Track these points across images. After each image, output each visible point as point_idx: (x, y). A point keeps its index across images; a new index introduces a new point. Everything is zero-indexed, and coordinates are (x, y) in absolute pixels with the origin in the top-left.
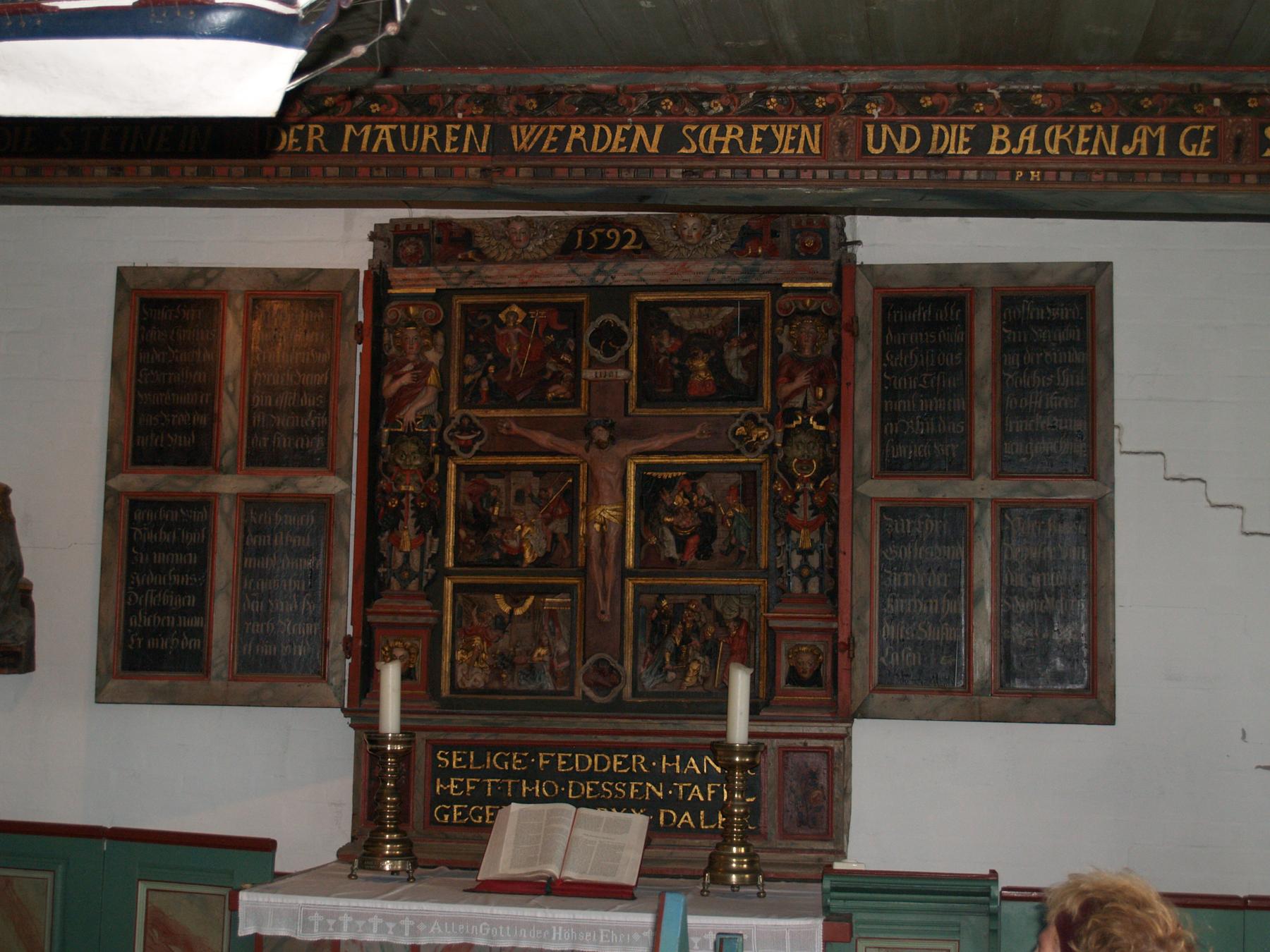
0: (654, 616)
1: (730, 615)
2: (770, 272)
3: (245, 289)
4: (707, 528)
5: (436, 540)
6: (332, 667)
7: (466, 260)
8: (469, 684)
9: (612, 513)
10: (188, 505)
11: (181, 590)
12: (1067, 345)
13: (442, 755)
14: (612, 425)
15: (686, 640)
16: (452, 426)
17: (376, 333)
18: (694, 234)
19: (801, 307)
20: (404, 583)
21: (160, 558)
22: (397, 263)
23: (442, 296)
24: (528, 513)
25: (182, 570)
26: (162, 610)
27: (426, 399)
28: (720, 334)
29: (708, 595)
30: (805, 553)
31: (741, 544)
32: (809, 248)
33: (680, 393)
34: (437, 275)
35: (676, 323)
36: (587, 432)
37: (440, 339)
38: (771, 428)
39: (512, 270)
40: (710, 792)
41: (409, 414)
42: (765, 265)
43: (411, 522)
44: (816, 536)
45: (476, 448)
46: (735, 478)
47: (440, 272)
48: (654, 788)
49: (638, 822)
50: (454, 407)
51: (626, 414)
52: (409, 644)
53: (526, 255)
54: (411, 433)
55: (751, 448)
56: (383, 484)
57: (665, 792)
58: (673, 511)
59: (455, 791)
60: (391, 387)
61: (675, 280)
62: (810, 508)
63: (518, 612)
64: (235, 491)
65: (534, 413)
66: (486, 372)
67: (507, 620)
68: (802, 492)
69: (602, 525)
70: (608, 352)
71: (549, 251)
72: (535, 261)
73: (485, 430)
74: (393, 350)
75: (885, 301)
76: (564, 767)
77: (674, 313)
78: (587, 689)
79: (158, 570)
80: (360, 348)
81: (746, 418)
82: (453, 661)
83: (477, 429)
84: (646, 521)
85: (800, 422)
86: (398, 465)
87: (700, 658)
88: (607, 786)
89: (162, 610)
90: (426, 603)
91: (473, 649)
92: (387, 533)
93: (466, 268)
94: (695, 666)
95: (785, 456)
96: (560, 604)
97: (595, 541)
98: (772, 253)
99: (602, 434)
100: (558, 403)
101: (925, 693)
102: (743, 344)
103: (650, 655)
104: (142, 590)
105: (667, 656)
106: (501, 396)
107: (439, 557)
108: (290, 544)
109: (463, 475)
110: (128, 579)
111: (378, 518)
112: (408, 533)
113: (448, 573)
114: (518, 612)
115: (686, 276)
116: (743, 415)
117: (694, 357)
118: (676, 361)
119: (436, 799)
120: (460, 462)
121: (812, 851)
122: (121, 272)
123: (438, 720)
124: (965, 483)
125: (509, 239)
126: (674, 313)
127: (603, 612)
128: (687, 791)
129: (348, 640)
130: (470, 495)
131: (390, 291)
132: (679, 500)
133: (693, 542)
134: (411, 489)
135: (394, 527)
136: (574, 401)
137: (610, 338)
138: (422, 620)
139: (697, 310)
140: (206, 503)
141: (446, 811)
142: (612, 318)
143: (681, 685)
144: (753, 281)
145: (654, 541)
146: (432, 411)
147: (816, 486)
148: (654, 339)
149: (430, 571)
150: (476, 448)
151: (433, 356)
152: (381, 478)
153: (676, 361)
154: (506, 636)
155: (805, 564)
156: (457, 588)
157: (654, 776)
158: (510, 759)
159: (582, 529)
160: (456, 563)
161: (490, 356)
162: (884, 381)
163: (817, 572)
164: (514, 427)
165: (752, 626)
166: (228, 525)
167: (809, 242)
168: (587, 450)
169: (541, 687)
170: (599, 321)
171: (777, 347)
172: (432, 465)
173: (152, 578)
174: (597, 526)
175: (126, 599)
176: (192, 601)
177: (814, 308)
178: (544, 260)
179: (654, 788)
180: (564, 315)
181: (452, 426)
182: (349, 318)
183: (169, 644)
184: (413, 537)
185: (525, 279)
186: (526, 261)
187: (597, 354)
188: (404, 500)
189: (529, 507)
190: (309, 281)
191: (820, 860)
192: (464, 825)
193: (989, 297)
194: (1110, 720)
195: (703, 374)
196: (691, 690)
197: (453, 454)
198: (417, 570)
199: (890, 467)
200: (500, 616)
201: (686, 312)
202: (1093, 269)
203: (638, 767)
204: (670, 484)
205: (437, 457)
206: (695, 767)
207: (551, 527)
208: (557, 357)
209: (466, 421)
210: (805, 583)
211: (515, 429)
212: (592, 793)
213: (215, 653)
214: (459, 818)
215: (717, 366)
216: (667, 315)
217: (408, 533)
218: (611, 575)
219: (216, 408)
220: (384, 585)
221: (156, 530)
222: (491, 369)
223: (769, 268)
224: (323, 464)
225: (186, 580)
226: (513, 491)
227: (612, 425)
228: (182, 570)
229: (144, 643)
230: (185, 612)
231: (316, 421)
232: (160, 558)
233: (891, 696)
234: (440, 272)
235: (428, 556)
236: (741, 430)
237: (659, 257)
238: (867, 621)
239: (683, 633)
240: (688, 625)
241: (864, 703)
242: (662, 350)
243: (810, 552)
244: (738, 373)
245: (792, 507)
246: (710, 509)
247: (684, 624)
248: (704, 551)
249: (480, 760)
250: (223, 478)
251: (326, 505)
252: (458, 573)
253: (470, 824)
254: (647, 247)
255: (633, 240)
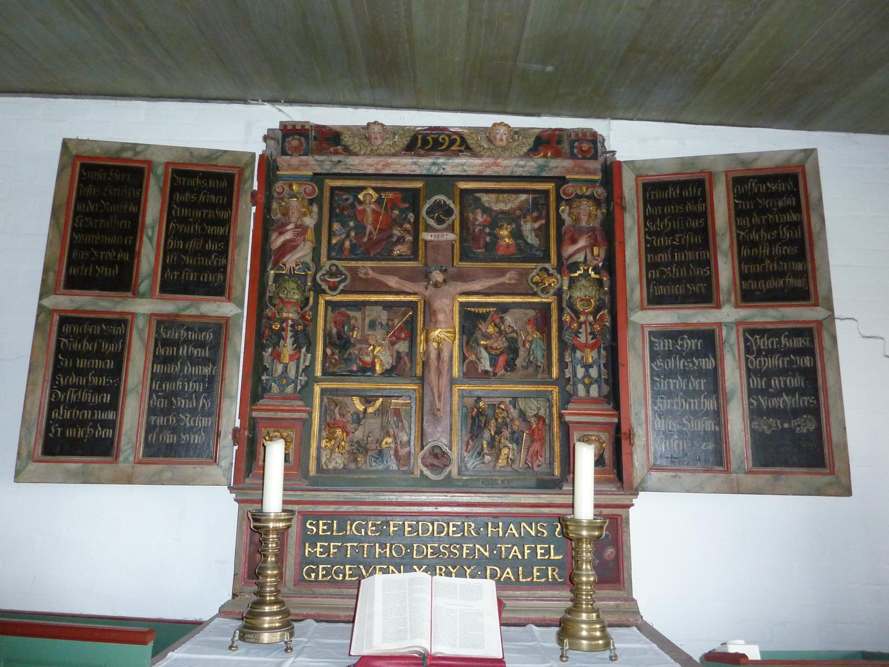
0: (474, 413)
1: (530, 413)
2: (556, 167)
3: (165, 160)
4: (513, 349)
5: (309, 355)
6: (221, 453)
7: (336, 153)
8: (331, 466)
9: (444, 335)
10: (108, 322)
11: (98, 390)
12: (784, 210)
13: (311, 524)
14: (446, 270)
15: (498, 432)
16: (323, 272)
17: (265, 201)
18: (504, 137)
19: (580, 193)
20: (282, 387)
21: (81, 363)
22: (284, 153)
23: (318, 178)
24: (378, 337)
25: (100, 373)
26: (81, 405)
27: (303, 252)
28: (518, 213)
29: (513, 398)
30: (587, 367)
31: (537, 361)
32: (584, 151)
33: (491, 251)
34: (314, 163)
35: (487, 205)
36: (427, 276)
37: (315, 208)
38: (559, 277)
39: (370, 160)
40: (527, 552)
41: (291, 260)
42: (553, 163)
43: (289, 341)
44: (594, 354)
45: (341, 287)
46: (531, 313)
47: (316, 160)
48: (481, 549)
49: (488, 586)
50: (324, 259)
51: (453, 266)
52: (285, 434)
53: (381, 151)
54: (292, 275)
55: (545, 291)
56: (268, 312)
57: (491, 552)
58: (487, 337)
59: (321, 553)
60: (277, 241)
61: (488, 172)
62: (590, 334)
63: (370, 410)
64: (149, 312)
65: (384, 264)
66: (348, 236)
67: (361, 416)
68: (585, 322)
69: (439, 344)
70: (440, 221)
71: (397, 149)
72: (386, 155)
73: (348, 274)
74: (279, 216)
75: (646, 186)
76: (409, 532)
77: (485, 198)
78: (424, 469)
79: (81, 372)
80: (254, 209)
81: (541, 270)
82: (319, 448)
83: (342, 274)
84: (468, 343)
85: (581, 272)
86: (281, 298)
87: (510, 445)
88: (444, 548)
89: (81, 405)
90: (300, 403)
91: (335, 438)
92: (270, 350)
93: (335, 158)
94: (505, 451)
95: (570, 297)
96: (403, 405)
97: (433, 355)
98: (558, 154)
99: (438, 276)
100: (401, 257)
101: (693, 472)
102: (535, 220)
103: (471, 443)
104: (64, 389)
105: (485, 443)
106: (355, 253)
107: (309, 370)
108: (192, 354)
109: (330, 308)
110: (54, 379)
111: (262, 337)
112: (287, 348)
113: (317, 380)
114: (370, 410)
115: (496, 169)
116: (539, 268)
117: (501, 227)
118: (488, 230)
119: (304, 561)
120: (328, 298)
121: (610, 599)
122: (65, 143)
123: (308, 496)
124: (716, 312)
125: (368, 139)
126: (485, 198)
127: (438, 410)
128: (508, 550)
129: (235, 430)
130: (335, 323)
131: (278, 173)
132: (491, 330)
133: (502, 360)
134: (291, 315)
135: (276, 345)
136: (414, 256)
137: (441, 212)
138: (297, 415)
139: (501, 196)
140: (123, 322)
141: (313, 571)
142: (441, 198)
143: (495, 466)
144: (544, 174)
145: (473, 358)
146: (308, 259)
147: (594, 318)
148: (471, 216)
149: (303, 378)
150: (341, 287)
151: (310, 221)
152: (267, 307)
153: (488, 230)
154: (361, 429)
155: (587, 375)
156: (323, 392)
157: (493, 543)
158: (366, 527)
159: (421, 348)
160: (324, 373)
161: (352, 224)
162: (647, 241)
163: (596, 381)
164: (370, 272)
165: (547, 421)
166: (142, 339)
167: (585, 147)
168: (427, 288)
169: (388, 467)
170: (433, 200)
171: (560, 222)
172: (307, 299)
173: (74, 379)
174: (435, 344)
175: (51, 396)
176: (107, 398)
177: (588, 193)
178: (394, 155)
179: (481, 549)
180: (408, 199)
181: (323, 272)
182: (247, 186)
183: (85, 433)
184: (292, 352)
185: (380, 167)
186: (380, 155)
187: (431, 222)
188: (284, 325)
189: (379, 334)
190: (217, 158)
191: (617, 606)
192: (328, 581)
193: (723, 178)
194: (846, 491)
195: (507, 240)
196: (503, 469)
197: (324, 292)
198: (293, 378)
199: (655, 300)
200: (357, 413)
201: (493, 196)
202: (803, 154)
203: (469, 531)
204: (484, 317)
205: (312, 293)
206: (514, 531)
207: (396, 347)
208: (401, 226)
209: (334, 268)
210: (587, 388)
211: (372, 274)
212: (432, 554)
213: (124, 439)
214: (323, 576)
215: (517, 234)
216: (480, 200)
217: (287, 348)
218: (445, 380)
219: (137, 248)
220: (266, 389)
221: (80, 341)
222: (353, 234)
223: (555, 165)
224: (221, 293)
225: (103, 381)
226: (367, 321)
227: (446, 270)
228: (100, 373)
229: (63, 433)
230: (102, 407)
231: (218, 262)
232: (81, 363)
233: (665, 474)
234: (316, 160)
235: (302, 367)
236: (537, 279)
237: (475, 155)
238: (643, 416)
239: (497, 427)
240: (499, 420)
241: (643, 481)
242: (477, 223)
243: (591, 366)
244: (532, 239)
245: (577, 333)
246: (515, 335)
247: (496, 420)
248: (510, 366)
249: (342, 528)
250: (138, 300)
251: (220, 329)
252: (324, 381)
253: (333, 582)
254: (468, 148)
255: (458, 142)
